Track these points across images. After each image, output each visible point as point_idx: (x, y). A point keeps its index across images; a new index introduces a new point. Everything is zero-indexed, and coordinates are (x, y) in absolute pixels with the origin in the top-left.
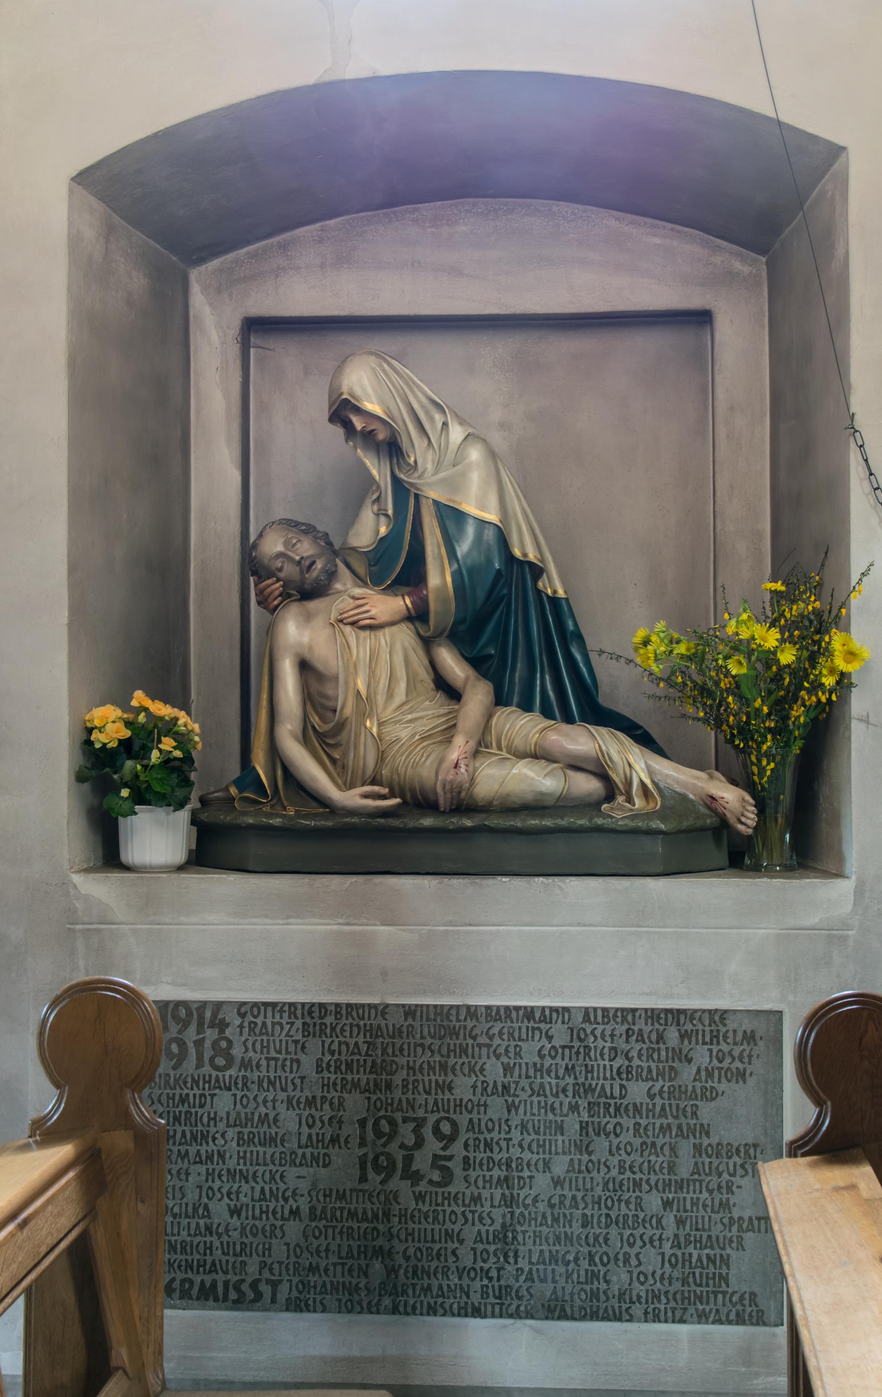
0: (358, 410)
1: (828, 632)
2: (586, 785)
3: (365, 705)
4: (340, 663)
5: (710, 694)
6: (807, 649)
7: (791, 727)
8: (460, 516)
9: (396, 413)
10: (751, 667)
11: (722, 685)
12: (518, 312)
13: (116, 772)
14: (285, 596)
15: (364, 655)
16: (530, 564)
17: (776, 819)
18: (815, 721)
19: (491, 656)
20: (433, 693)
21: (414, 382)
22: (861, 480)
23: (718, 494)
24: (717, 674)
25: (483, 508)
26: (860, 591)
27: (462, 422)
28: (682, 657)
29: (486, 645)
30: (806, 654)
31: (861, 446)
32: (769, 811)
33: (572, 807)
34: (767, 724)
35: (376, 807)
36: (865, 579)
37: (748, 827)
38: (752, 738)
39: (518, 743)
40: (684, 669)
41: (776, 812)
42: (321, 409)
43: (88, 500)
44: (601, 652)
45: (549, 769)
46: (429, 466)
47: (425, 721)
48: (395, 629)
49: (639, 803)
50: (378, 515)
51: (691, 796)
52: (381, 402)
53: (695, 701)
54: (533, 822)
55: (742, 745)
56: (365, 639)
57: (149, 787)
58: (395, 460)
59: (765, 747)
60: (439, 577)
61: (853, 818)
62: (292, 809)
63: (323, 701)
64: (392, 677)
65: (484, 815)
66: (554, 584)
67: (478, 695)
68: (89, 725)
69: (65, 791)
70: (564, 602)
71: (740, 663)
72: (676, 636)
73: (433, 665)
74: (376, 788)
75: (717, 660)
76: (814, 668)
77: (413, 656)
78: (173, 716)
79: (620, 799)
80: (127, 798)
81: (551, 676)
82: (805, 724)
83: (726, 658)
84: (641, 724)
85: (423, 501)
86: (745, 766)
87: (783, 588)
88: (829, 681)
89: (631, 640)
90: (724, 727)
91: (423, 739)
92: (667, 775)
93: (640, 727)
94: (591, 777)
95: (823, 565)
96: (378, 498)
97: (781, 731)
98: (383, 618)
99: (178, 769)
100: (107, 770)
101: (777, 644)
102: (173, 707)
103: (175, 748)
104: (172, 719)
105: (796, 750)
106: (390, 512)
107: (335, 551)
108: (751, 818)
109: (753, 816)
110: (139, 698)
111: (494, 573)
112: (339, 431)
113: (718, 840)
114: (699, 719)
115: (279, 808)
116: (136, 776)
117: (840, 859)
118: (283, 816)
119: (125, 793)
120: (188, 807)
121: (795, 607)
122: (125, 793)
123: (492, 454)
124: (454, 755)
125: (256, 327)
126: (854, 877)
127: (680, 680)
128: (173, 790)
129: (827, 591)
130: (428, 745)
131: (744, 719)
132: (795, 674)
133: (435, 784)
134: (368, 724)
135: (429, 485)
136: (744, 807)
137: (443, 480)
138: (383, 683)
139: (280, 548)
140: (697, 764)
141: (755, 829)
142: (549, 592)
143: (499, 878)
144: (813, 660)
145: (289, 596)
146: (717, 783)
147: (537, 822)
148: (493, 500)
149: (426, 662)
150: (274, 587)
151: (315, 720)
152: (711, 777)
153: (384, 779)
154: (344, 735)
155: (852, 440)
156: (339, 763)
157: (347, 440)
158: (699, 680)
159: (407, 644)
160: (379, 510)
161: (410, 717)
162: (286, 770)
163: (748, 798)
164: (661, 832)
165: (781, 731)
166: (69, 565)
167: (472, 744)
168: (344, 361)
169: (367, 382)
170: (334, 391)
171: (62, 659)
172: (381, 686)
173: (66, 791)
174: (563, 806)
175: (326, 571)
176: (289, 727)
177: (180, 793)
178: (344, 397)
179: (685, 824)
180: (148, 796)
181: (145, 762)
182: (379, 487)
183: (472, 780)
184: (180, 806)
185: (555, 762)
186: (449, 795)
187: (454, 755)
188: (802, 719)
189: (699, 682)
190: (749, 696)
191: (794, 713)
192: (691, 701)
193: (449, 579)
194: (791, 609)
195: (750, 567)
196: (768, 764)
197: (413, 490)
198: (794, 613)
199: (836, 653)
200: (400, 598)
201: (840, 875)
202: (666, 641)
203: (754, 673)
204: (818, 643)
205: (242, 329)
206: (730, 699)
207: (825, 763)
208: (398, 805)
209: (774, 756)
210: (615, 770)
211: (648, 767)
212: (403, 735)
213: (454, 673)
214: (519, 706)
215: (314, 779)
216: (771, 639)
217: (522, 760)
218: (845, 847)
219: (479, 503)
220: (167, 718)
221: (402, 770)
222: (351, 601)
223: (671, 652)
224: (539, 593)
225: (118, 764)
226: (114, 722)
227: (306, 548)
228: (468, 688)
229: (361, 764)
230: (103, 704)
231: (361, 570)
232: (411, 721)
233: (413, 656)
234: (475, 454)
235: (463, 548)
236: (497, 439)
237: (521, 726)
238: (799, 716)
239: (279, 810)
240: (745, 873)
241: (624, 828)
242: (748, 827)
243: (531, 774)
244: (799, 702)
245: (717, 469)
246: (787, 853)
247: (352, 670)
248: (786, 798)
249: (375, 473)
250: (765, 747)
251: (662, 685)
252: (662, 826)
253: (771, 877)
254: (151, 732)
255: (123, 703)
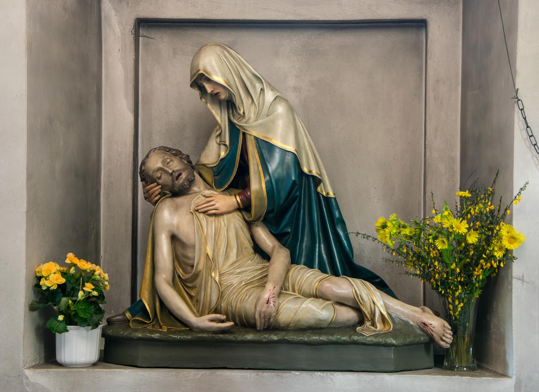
0: (209, 80)
1: (498, 224)
2: (347, 315)
3: (211, 262)
4: (196, 237)
5: (423, 259)
6: (485, 234)
7: (474, 282)
8: (271, 147)
9: (232, 83)
10: (450, 245)
11: (431, 255)
12: (307, 19)
13: (55, 305)
14: (163, 194)
15: (210, 231)
16: (313, 177)
17: (464, 338)
18: (489, 277)
19: (288, 233)
20: (253, 255)
21: (243, 64)
22: (521, 130)
23: (428, 134)
24: (429, 248)
25: (285, 142)
26: (519, 200)
27: (273, 89)
28: (406, 236)
29: (286, 226)
30: (484, 237)
31: (522, 109)
32: (460, 333)
33: (339, 328)
34: (459, 279)
35: (219, 328)
36: (522, 192)
37: (447, 343)
38: (450, 288)
39: (306, 288)
40: (407, 244)
41: (464, 334)
42: (184, 78)
43: (40, 133)
44: (358, 234)
45: (324, 305)
46: (252, 115)
47: (248, 273)
48: (230, 216)
49: (379, 326)
50: (220, 144)
51: (411, 323)
52: (224, 76)
53: (415, 264)
54: (314, 338)
55: (443, 292)
56: (212, 222)
57: (76, 314)
58: (231, 111)
59: (457, 294)
60: (257, 184)
61: (514, 340)
62: (165, 327)
63: (186, 260)
64: (228, 246)
65: (284, 333)
66: (327, 189)
67: (281, 257)
68: (38, 275)
69: (22, 317)
70: (333, 200)
71: (443, 242)
72: (402, 223)
73: (253, 238)
74: (218, 316)
75: (428, 240)
76: (489, 245)
77: (240, 232)
78: (92, 269)
79: (368, 324)
80: (62, 321)
81: (325, 246)
82: (483, 280)
83: (435, 238)
84: (378, 274)
85: (248, 137)
86: (444, 304)
87: (470, 195)
88: (499, 254)
89: (372, 222)
90: (432, 280)
91: (247, 285)
92: (397, 309)
93: (379, 277)
94: (350, 310)
95: (494, 181)
96: (220, 134)
97: (467, 284)
98: (223, 209)
99: (94, 303)
100: (50, 303)
101: (467, 231)
102: (92, 263)
103: (93, 290)
104: (91, 271)
105: (476, 295)
106: (227, 143)
107: (193, 166)
108: (449, 338)
109: (450, 336)
110: (71, 258)
111: (291, 182)
112: (196, 92)
113: (427, 349)
114: (416, 275)
115: (158, 327)
116: (68, 307)
117: (505, 365)
118: (160, 332)
119: (61, 318)
120: (101, 326)
121: (477, 208)
122: (61, 318)
123: (291, 109)
124: (266, 295)
125: (144, 24)
126: (514, 377)
127: (405, 251)
128: (91, 316)
129: (497, 198)
130: (250, 288)
131: (445, 276)
132: (477, 248)
133: (255, 313)
134: (213, 275)
135: (252, 127)
136: (444, 331)
137: (261, 125)
138: (223, 249)
139: (160, 165)
140: (412, 302)
141: (451, 344)
142: (324, 194)
143: (293, 372)
144: (488, 241)
145: (165, 194)
146: (427, 315)
147: (317, 338)
148: (291, 138)
149: (249, 236)
150: (155, 189)
151: (180, 271)
152: (424, 311)
153: (223, 309)
154: (198, 282)
155: (516, 105)
156: (195, 299)
157: (201, 98)
158: (416, 249)
159: (237, 225)
160: (220, 141)
161: (239, 270)
162: (162, 303)
163: (447, 325)
164: (393, 345)
165: (467, 284)
166: (27, 174)
167: (278, 288)
168: (200, 49)
169: (215, 64)
170: (194, 67)
171: (23, 233)
172: (221, 251)
173: (23, 317)
174: (333, 328)
175: (188, 180)
176: (164, 276)
177: (95, 318)
178: (201, 72)
179: (408, 340)
180: (76, 320)
181: (74, 298)
182: (220, 127)
183: (277, 311)
184: (96, 326)
185: (328, 300)
186: (263, 320)
187: (266, 295)
188: (481, 277)
189: (416, 251)
190: (448, 262)
191: (476, 273)
192: (412, 264)
193: (264, 186)
194: (475, 209)
195: (446, 180)
196: (459, 303)
197: (242, 130)
198: (476, 211)
199: (503, 238)
200: (234, 197)
201: (504, 375)
202: (396, 226)
203: (451, 248)
204: (492, 230)
205: (135, 26)
206: (436, 263)
207: (495, 304)
208: (232, 326)
209: (463, 299)
210: (364, 306)
211: (385, 304)
212: (235, 282)
213: (266, 243)
214: (305, 264)
215: (179, 309)
216: (462, 227)
217: (306, 297)
218: (508, 358)
219: (283, 139)
220: (88, 271)
221: (234, 304)
222: (203, 198)
223: (399, 233)
224: (318, 194)
225: (57, 300)
226: (54, 273)
227: (176, 165)
228: (275, 253)
229: (208, 299)
230: (47, 261)
231: (209, 178)
232: (239, 273)
233: (240, 232)
234: (281, 109)
235: (273, 166)
236: (292, 97)
237: (308, 277)
238: (479, 275)
239: (157, 328)
240: (445, 372)
241: (371, 343)
242: (447, 343)
243: (314, 308)
244: (479, 266)
245: (427, 118)
246: (471, 358)
247: (203, 241)
248: (470, 325)
249: (218, 118)
250: (457, 294)
251: (394, 254)
252: (394, 342)
253: (462, 375)
254: (78, 279)
255: (61, 261)
